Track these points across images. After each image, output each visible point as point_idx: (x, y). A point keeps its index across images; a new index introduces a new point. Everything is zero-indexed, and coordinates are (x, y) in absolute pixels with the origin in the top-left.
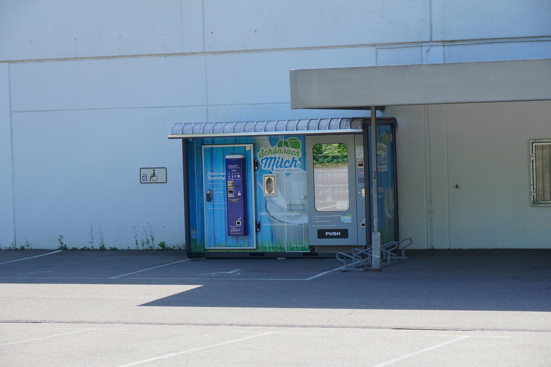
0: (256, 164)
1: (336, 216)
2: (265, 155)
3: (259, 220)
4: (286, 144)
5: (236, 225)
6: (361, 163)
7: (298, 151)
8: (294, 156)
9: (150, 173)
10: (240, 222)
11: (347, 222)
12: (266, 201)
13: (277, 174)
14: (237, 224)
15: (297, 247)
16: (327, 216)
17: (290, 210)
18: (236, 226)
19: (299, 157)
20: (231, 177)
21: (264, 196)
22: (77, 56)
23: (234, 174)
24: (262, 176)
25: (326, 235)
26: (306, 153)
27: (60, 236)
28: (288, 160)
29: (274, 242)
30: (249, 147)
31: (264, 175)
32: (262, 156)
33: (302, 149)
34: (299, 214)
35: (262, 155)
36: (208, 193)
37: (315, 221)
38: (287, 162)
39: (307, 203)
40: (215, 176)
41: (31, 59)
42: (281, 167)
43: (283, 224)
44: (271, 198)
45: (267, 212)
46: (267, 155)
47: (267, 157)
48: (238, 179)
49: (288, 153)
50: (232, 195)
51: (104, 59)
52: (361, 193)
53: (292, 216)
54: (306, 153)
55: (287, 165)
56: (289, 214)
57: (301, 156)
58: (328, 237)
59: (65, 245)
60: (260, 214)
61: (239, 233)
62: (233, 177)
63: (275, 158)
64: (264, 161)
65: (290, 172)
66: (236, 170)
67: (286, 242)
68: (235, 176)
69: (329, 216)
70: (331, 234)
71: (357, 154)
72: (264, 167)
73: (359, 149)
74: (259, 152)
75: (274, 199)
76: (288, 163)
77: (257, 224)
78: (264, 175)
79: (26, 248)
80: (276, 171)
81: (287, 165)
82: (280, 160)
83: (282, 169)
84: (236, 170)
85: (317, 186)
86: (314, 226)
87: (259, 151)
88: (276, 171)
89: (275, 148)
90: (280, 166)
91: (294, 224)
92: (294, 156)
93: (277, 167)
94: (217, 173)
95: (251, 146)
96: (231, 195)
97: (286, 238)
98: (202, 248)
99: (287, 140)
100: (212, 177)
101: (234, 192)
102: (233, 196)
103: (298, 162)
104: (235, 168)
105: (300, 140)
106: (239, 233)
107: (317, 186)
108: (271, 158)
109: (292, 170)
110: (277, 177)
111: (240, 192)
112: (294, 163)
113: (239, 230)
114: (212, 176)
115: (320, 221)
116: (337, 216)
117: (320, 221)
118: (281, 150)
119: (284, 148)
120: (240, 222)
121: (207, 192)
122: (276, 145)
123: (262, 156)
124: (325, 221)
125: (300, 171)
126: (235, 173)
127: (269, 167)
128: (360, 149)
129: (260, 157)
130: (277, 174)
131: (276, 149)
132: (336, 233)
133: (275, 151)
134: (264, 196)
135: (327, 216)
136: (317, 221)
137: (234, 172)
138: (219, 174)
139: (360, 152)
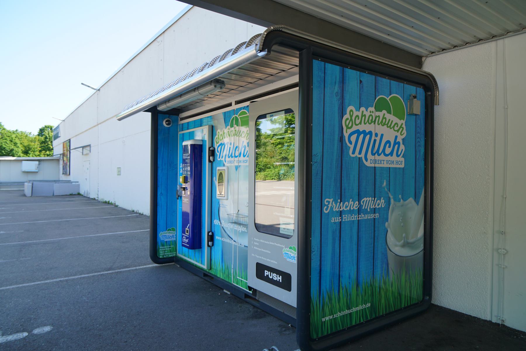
0: (212, 153)
2: (356, 125)
15: (241, 280)
25: (265, 275)
29: (223, 264)
46: (358, 125)
47: (358, 130)
55: (171, 237)
63: (166, 235)
82: (378, 139)
89: (370, 112)
93: (167, 239)
108: (164, 236)
115: (260, 249)
119: (235, 128)
123: (350, 126)
127: (360, 153)
129: (348, 128)
131: (372, 114)
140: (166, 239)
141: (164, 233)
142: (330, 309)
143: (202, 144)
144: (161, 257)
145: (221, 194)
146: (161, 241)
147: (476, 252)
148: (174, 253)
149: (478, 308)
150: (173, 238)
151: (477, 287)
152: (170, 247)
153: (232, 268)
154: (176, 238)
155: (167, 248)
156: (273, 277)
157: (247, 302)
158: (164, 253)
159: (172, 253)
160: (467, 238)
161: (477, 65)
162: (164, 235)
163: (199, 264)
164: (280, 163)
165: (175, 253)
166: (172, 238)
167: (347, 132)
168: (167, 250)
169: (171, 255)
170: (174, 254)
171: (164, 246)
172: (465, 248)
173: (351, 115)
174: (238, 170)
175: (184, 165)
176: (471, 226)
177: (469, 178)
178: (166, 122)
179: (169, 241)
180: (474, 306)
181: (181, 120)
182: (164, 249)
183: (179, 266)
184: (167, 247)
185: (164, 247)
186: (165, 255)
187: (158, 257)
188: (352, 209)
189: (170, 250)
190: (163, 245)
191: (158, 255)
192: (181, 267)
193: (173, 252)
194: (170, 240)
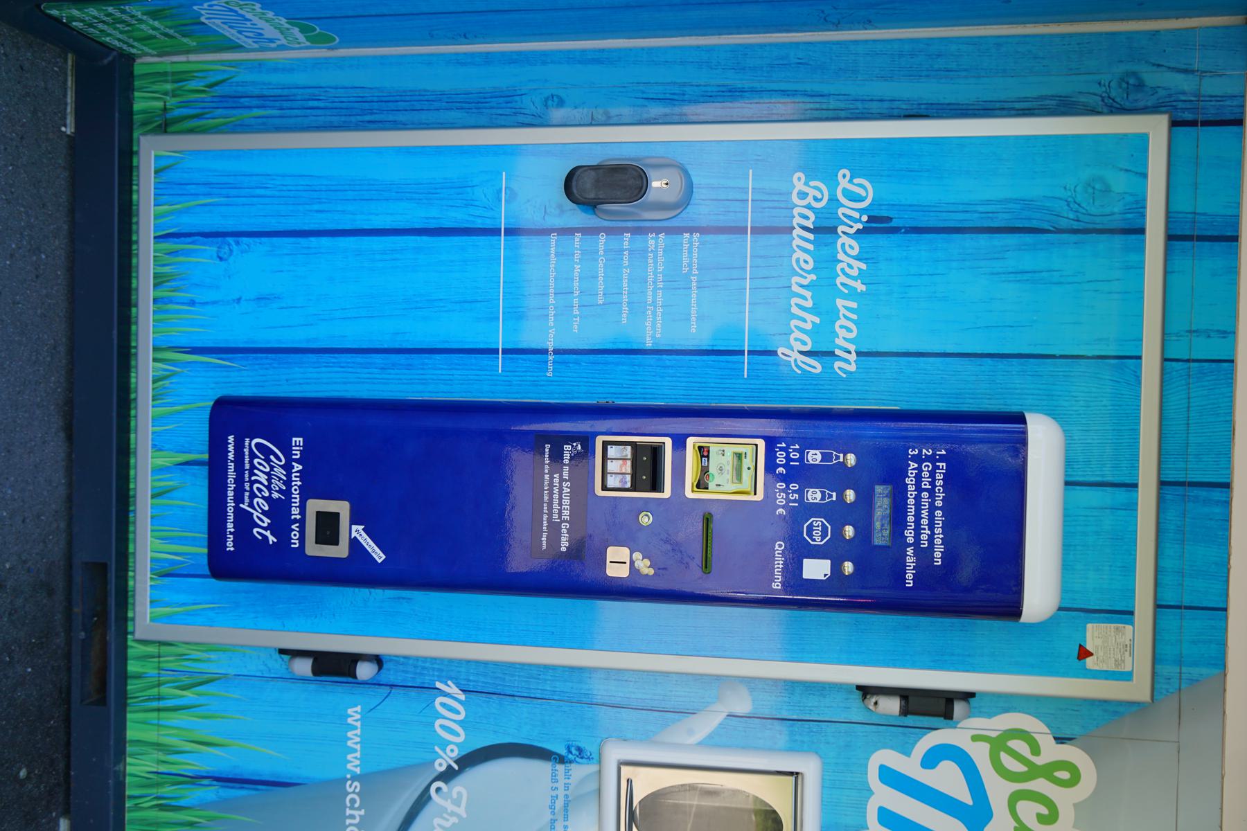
5: (305, 495)
9: (706, 454)
12: (562, 760)
14: (319, 515)
23: (835, 513)
24: (794, 748)
29: (210, 793)
31: (810, 767)
32: (1005, 759)
35: (1018, 767)
36: (655, 184)
40: (826, 264)
45: (469, 760)
48: (779, 563)
61: (230, 527)
62: (814, 495)
64: (948, 779)
66: (881, 536)
68: (817, 530)
72: (890, 777)
74: (1047, 742)
77: (355, 662)
78: (810, 767)
84: (881, 536)
87: (1060, 740)
95: (1127, 676)
96: (612, 466)
98: (171, 102)
100: (815, 230)
101: (646, 505)
102: (599, 492)
104: (909, 535)
106: (230, 527)
111: (644, 566)
113: (262, 528)
120: (335, 542)
121: (663, 165)
123: (1005, 759)
126: (849, 531)
129: (998, 744)
137: (862, 513)
138: (840, 303)
167: (975, 738)
183: (69, 129)
188: (794, 323)
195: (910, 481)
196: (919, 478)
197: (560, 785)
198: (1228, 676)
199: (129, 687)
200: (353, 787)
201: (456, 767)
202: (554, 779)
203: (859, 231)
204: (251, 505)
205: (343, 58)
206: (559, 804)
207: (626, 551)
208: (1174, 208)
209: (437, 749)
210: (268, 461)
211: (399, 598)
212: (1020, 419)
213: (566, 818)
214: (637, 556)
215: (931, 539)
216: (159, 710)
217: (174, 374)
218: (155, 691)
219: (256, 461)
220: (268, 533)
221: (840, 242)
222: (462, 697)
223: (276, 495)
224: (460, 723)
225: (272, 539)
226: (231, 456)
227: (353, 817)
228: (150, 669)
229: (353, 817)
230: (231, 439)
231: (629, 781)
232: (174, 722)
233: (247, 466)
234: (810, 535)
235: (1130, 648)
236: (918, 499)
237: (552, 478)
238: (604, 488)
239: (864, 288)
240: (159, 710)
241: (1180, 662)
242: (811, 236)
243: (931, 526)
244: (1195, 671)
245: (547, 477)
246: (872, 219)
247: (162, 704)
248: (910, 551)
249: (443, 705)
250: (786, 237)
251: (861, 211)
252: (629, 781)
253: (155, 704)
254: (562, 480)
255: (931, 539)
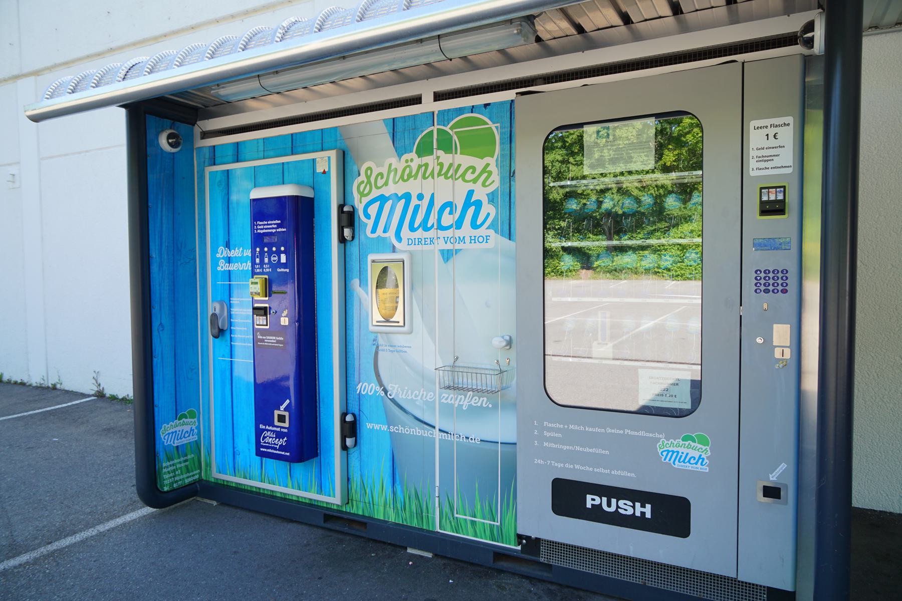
0: (348, 218)
1: (634, 433)
2: (378, 188)
3: (353, 407)
4: (446, 145)
6: (772, 197)
7: (488, 165)
8: (471, 186)
10: (287, 414)
11: (690, 467)
12: (377, 347)
13: (411, 255)
15: (473, 523)
16: (597, 430)
17: (453, 388)
18: (275, 429)
19: (490, 189)
20: (262, 261)
21: (371, 328)
22: (113, 45)
23: (270, 253)
25: (589, 506)
26: (516, 174)
27: (95, 372)
28: (452, 201)
29: (398, 488)
30: (327, 161)
32: (365, 192)
33: (503, 156)
34: (483, 401)
37: (546, 444)
38: (448, 209)
39: (514, 364)
41: (57, 62)
42: (426, 229)
43: (426, 432)
44: (391, 335)
49: (452, 176)
50: (265, 323)
51: (150, 45)
52: (769, 339)
53: (460, 406)
54: (514, 173)
55: (447, 220)
56: (450, 397)
57: (496, 185)
58: (597, 515)
59: (103, 388)
60: (359, 386)
61: (283, 453)
62: (266, 260)
64: (373, 210)
65: (457, 246)
67: (437, 499)
69: (603, 430)
70: (609, 505)
71: (752, 153)
72: (374, 231)
73: (764, 131)
74: (360, 179)
75: (400, 340)
76: (450, 214)
79: (58, 386)
80: (411, 242)
81: (447, 220)
83: (431, 234)
85: (554, 299)
86: (540, 462)
88: (411, 242)
90: (425, 226)
91: (467, 438)
92: (471, 186)
94: (238, 249)
95: (329, 158)
97: (437, 484)
99: (447, 129)
102: (268, 327)
103: (488, 209)
104: (274, 231)
105: (494, 123)
106: (283, 453)
107: (554, 299)
108: (172, 433)
109: (463, 240)
110: (412, 264)
111: (285, 313)
112: (192, 432)
113: (282, 442)
114: (229, 260)
115: (565, 448)
116: (642, 433)
117: (565, 448)
118: (426, 165)
119: (438, 158)
122: (411, 152)
123: (365, 192)
124: (587, 450)
125: (491, 244)
127: (170, 442)
128: (771, 132)
130: (411, 255)
132: (634, 507)
133: (678, 445)
134: (371, 328)
135: (597, 430)
136: (553, 445)
138: (245, 255)
139: (772, 142)
140: (176, 441)
141: (171, 425)
142: (454, 527)
143: (313, 197)
144: (166, 489)
145: (388, 321)
146: (165, 448)
147: (885, 400)
148: (195, 472)
149: (887, 495)
150: (191, 437)
151: (886, 460)
152: (185, 458)
153: (437, 495)
154: (199, 434)
155: (180, 463)
156: (618, 507)
157: (501, 571)
158: (174, 477)
159: (191, 474)
160: (865, 376)
161: (889, 69)
162: (170, 431)
163: (311, 495)
164: (605, 243)
165: (198, 471)
166: (189, 436)
168: (181, 468)
169: (190, 479)
170: (196, 474)
171: (173, 460)
172: (862, 393)
173: (369, 174)
174: (451, 260)
175: (258, 249)
176: (875, 355)
177: (871, 271)
178: (169, 137)
179: (183, 445)
180: (879, 493)
181: (202, 138)
182: (172, 468)
183: (215, 503)
184: (178, 461)
185: (171, 463)
186: (176, 482)
187: (162, 491)
189: (187, 466)
190: (170, 459)
191: (159, 486)
192: (223, 503)
193: (192, 471)
194: (184, 441)
195: (262, 232)
196: (261, 229)
197: (385, 348)
198: (340, 125)
199: (367, 515)
200: (392, 429)
201: (382, 388)
202: (383, 350)
203: (229, 250)
204: (277, 445)
205: (202, 409)
206: (391, 349)
207: (282, 318)
208: (231, 161)
209: (377, 395)
210: (266, 437)
211: (323, 402)
212: (251, 200)
213: (395, 346)
214: (283, 315)
215: (274, 224)
216: (373, 504)
217: (268, 476)
218: (367, 504)
219: (267, 442)
220: (284, 440)
221: (232, 256)
222: (361, 383)
223: (274, 436)
224: (369, 385)
225: (285, 439)
226: (266, 450)
227: (402, 430)
228: (361, 505)
229: (402, 430)
230: (261, 449)
231: (377, 322)
232: (377, 499)
233: (267, 445)
234: (275, 261)
235: (322, 158)
236: (266, 229)
237: (266, 342)
238: (267, 325)
239: (241, 248)
240: (373, 504)
241: (336, 141)
242: (231, 264)
243: (271, 224)
244: (338, 135)
245: (266, 344)
246: (227, 247)
247: (371, 503)
248: (278, 230)
249: (364, 391)
250: (231, 272)
251: (225, 250)
252: (377, 322)
253: (372, 505)
254: (266, 339)
255: (274, 224)
